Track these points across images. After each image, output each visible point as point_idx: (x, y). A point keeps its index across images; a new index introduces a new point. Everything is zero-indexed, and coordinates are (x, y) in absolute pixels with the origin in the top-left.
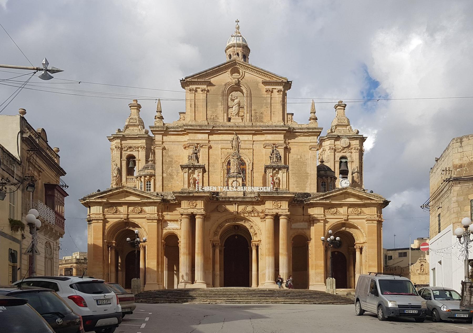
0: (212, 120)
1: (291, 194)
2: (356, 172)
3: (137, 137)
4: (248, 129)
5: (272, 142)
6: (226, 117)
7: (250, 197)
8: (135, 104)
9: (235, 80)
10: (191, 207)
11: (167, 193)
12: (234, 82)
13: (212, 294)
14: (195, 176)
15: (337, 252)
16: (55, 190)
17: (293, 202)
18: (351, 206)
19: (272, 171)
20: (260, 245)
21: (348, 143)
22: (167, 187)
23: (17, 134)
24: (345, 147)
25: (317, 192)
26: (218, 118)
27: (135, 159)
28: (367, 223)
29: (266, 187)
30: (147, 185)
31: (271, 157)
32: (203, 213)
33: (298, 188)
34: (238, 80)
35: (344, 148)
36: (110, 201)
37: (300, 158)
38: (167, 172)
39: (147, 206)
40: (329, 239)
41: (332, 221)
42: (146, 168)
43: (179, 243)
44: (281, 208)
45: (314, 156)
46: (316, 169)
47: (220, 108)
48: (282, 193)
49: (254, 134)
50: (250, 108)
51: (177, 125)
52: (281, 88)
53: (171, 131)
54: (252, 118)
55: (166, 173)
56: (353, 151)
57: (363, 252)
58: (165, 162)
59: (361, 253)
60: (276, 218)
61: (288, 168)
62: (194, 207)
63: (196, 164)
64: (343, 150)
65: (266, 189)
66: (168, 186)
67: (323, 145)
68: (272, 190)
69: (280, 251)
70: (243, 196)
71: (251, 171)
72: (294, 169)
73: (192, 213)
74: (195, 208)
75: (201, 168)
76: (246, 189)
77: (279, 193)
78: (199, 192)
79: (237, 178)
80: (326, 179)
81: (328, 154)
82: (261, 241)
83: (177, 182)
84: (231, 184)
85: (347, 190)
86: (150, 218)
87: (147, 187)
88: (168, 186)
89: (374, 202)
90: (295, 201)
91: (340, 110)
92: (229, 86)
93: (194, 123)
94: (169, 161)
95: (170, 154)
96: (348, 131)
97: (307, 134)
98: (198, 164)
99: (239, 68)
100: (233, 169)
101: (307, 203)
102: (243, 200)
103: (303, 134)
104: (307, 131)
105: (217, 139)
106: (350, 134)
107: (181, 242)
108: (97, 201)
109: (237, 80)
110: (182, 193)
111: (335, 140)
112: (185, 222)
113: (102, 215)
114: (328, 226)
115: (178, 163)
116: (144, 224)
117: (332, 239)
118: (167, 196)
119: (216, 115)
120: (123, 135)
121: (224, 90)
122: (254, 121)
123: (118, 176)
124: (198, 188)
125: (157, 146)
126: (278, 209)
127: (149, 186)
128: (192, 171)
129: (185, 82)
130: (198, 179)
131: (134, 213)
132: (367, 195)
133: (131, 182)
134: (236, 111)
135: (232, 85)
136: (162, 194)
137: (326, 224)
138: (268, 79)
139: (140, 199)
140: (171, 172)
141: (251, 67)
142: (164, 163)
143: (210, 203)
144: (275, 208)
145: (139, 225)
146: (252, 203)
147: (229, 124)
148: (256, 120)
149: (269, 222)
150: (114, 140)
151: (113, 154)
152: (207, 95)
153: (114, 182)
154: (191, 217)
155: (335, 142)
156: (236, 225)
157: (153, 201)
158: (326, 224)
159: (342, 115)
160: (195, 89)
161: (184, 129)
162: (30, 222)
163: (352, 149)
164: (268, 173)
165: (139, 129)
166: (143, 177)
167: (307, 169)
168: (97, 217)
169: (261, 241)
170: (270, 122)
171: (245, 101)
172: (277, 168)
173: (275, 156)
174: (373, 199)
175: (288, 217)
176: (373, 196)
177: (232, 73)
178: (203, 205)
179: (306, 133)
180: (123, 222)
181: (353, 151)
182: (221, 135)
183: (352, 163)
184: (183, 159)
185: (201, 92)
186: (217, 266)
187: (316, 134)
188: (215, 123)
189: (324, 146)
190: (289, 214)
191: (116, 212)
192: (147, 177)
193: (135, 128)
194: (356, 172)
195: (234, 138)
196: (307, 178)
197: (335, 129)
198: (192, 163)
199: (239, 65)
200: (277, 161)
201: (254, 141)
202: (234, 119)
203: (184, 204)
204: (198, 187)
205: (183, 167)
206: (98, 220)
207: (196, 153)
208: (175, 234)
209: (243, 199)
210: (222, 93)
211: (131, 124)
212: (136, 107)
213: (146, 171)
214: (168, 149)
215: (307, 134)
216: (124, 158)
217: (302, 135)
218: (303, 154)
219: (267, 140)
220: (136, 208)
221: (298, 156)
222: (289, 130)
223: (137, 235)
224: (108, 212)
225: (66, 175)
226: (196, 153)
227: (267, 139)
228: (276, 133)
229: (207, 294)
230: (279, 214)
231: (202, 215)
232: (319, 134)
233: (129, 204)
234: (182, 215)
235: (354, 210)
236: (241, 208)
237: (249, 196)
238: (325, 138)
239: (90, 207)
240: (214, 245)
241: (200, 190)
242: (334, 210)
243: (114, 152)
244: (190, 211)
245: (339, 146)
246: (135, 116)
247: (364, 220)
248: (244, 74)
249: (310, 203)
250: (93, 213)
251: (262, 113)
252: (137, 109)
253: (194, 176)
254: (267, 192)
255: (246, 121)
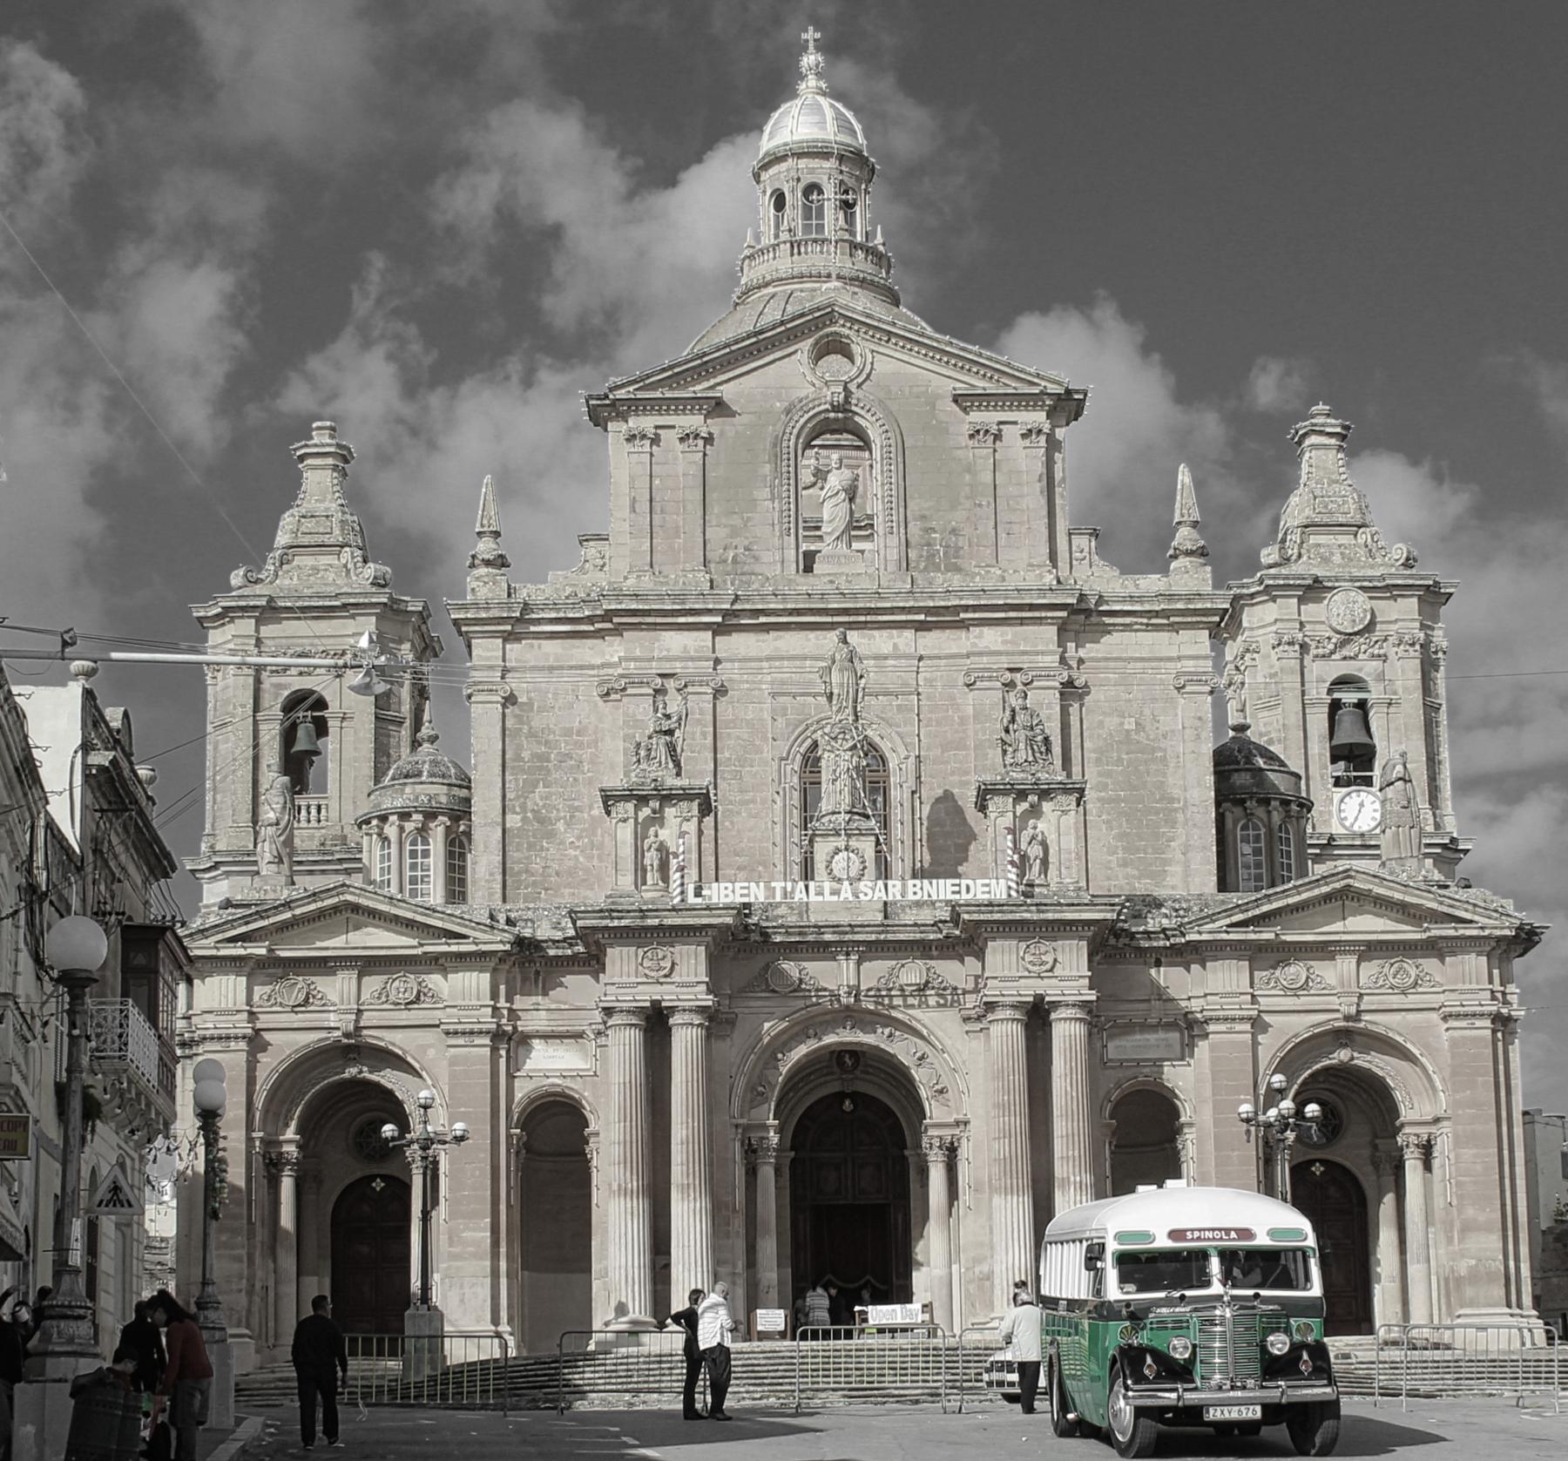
0: (729, 568)
1: (1101, 911)
2: (1400, 779)
3: (337, 603)
4: (895, 605)
5: (1003, 659)
6: (793, 552)
7: (916, 925)
8: (323, 445)
9: (833, 389)
10: (646, 975)
11: (536, 909)
12: (828, 398)
13: (781, 1368)
14: (666, 834)
15: (1322, 1162)
16: (160, 947)
17: (1112, 941)
18: (1371, 950)
19: (1010, 807)
20: (964, 1142)
21: (1365, 611)
22: (524, 876)
23: (72, 753)
24: (1355, 634)
25: (1223, 885)
26: (756, 558)
27: (325, 714)
28: (1447, 1029)
29: (987, 881)
30: (413, 854)
31: (1004, 742)
32: (708, 1000)
33: (1129, 870)
34: (845, 389)
35: (1348, 638)
36: (278, 952)
37: (1137, 731)
38: (523, 807)
39: (444, 971)
40: (1273, 1112)
41: (1290, 1027)
42: (406, 777)
43: (592, 1140)
44: (1057, 972)
45: (1200, 719)
46: (1209, 765)
47: (768, 507)
48: (1060, 904)
49: (921, 627)
50: (902, 510)
51: (569, 590)
52: (1038, 418)
53: (539, 621)
54: (913, 554)
55: (518, 809)
56: (1389, 649)
57: (1436, 1163)
58: (514, 760)
59: (1428, 1167)
60: (1037, 1016)
61: (1081, 791)
62: (666, 976)
63: (671, 781)
64: (1343, 644)
65: (987, 889)
66: (527, 871)
67: (1245, 624)
68: (1013, 893)
69: (1060, 1170)
70: (879, 917)
71: (913, 793)
72: (1109, 781)
73: (652, 1002)
74: (668, 980)
75: (692, 801)
76: (895, 890)
77: (1045, 905)
78: (687, 910)
79: (849, 836)
80: (1260, 812)
81: (1272, 667)
82: (966, 1123)
83: (572, 852)
84: (825, 864)
85: (1350, 881)
86: (460, 1027)
87: (413, 867)
88: (527, 871)
89: (1475, 933)
90: (1117, 936)
91: (1320, 452)
92: (807, 416)
93: (647, 583)
94: (535, 756)
95: (537, 722)
96: (1362, 552)
97: (1165, 621)
98: (678, 782)
99: (848, 337)
100: (835, 795)
101: (1172, 945)
102: (882, 937)
103: (1145, 621)
104: (1162, 606)
105: (753, 654)
106: (1372, 567)
107: (597, 1134)
108: (223, 952)
109: (840, 389)
110: (610, 913)
111: (1302, 600)
112: (625, 1043)
113: (246, 1014)
114: (1270, 1048)
115: (573, 762)
116: (431, 1053)
117: (1284, 1112)
118: (533, 922)
119: (746, 543)
120: (271, 599)
121: (784, 433)
122: (922, 565)
123: (283, 824)
124: (682, 892)
125: (480, 687)
126: (1042, 978)
127: (419, 860)
128: (654, 812)
129: (607, 402)
130: (681, 849)
131: (385, 1006)
132: (1441, 903)
133: (314, 824)
134: (835, 524)
135: (817, 410)
136: (513, 915)
137: (1260, 1038)
138: (982, 385)
139: (415, 942)
140: (544, 806)
141: (902, 333)
142: (509, 764)
143: (731, 954)
144: (1026, 974)
145: (409, 1059)
146: (923, 949)
147: (805, 584)
148: (932, 564)
149: (1007, 1033)
150: (223, 624)
151: (218, 688)
152: (705, 455)
153: (267, 849)
154: (648, 1019)
155: (1302, 607)
156: (846, 1051)
157: (473, 948)
158: (1260, 1038)
159: (1333, 477)
160: (650, 432)
161: (606, 611)
162: (209, 1108)
163: (1385, 640)
164: (993, 816)
165: (345, 566)
166: (393, 818)
167: (1171, 780)
168: (225, 1025)
169: (966, 1123)
170: (993, 570)
171: (879, 478)
172: (1033, 791)
173: (1022, 735)
174: (1471, 922)
175: (1090, 1012)
176: (1470, 907)
177: (821, 351)
178: (702, 968)
179: (1157, 617)
180: (337, 1048)
181: (1389, 649)
182: (773, 634)
183: (1392, 710)
184: (596, 747)
185: (680, 447)
186: (768, 1248)
187: (1204, 619)
188: (744, 578)
189: (1252, 629)
190: (1094, 998)
191: (306, 1002)
192: (415, 817)
193: (325, 560)
194: (1400, 779)
195: (838, 657)
196: (1173, 823)
197: (1301, 546)
198: (653, 775)
199: (848, 325)
200: (1031, 759)
201: (921, 659)
202: (830, 558)
203: (619, 959)
204: (682, 884)
205: (609, 799)
206: (228, 1038)
207: (670, 732)
208: (573, 1098)
209: (882, 932)
210: (775, 445)
211: (306, 540)
212: (330, 461)
213: (408, 790)
214: (530, 704)
215: (1165, 621)
216: (273, 706)
217: (1141, 624)
218: (1147, 712)
219: (980, 654)
220: (397, 982)
221: (1126, 721)
222: (1083, 606)
223: (393, 1108)
224: (273, 1001)
225: (174, 875)
226: (670, 732)
227: (982, 645)
228: (1022, 622)
229: (756, 1368)
230: (1047, 999)
231: (701, 1010)
232: (1217, 619)
233: (368, 965)
234: (609, 1012)
235: (1386, 970)
236: (875, 971)
237: (909, 917)
238: (1253, 590)
239: (190, 981)
240: (750, 1144)
241: (692, 900)
242: (1295, 971)
243: (224, 679)
244: (645, 994)
245: (1323, 627)
246: (327, 504)
247: (1434, 1016)
248: (872, 363)
249: (1188, 942)
250: (205, 1007)
251: (954, 531)
252: (335, 468)
253: (661, 838)
254: (990, 904)
255: (882, 567)
